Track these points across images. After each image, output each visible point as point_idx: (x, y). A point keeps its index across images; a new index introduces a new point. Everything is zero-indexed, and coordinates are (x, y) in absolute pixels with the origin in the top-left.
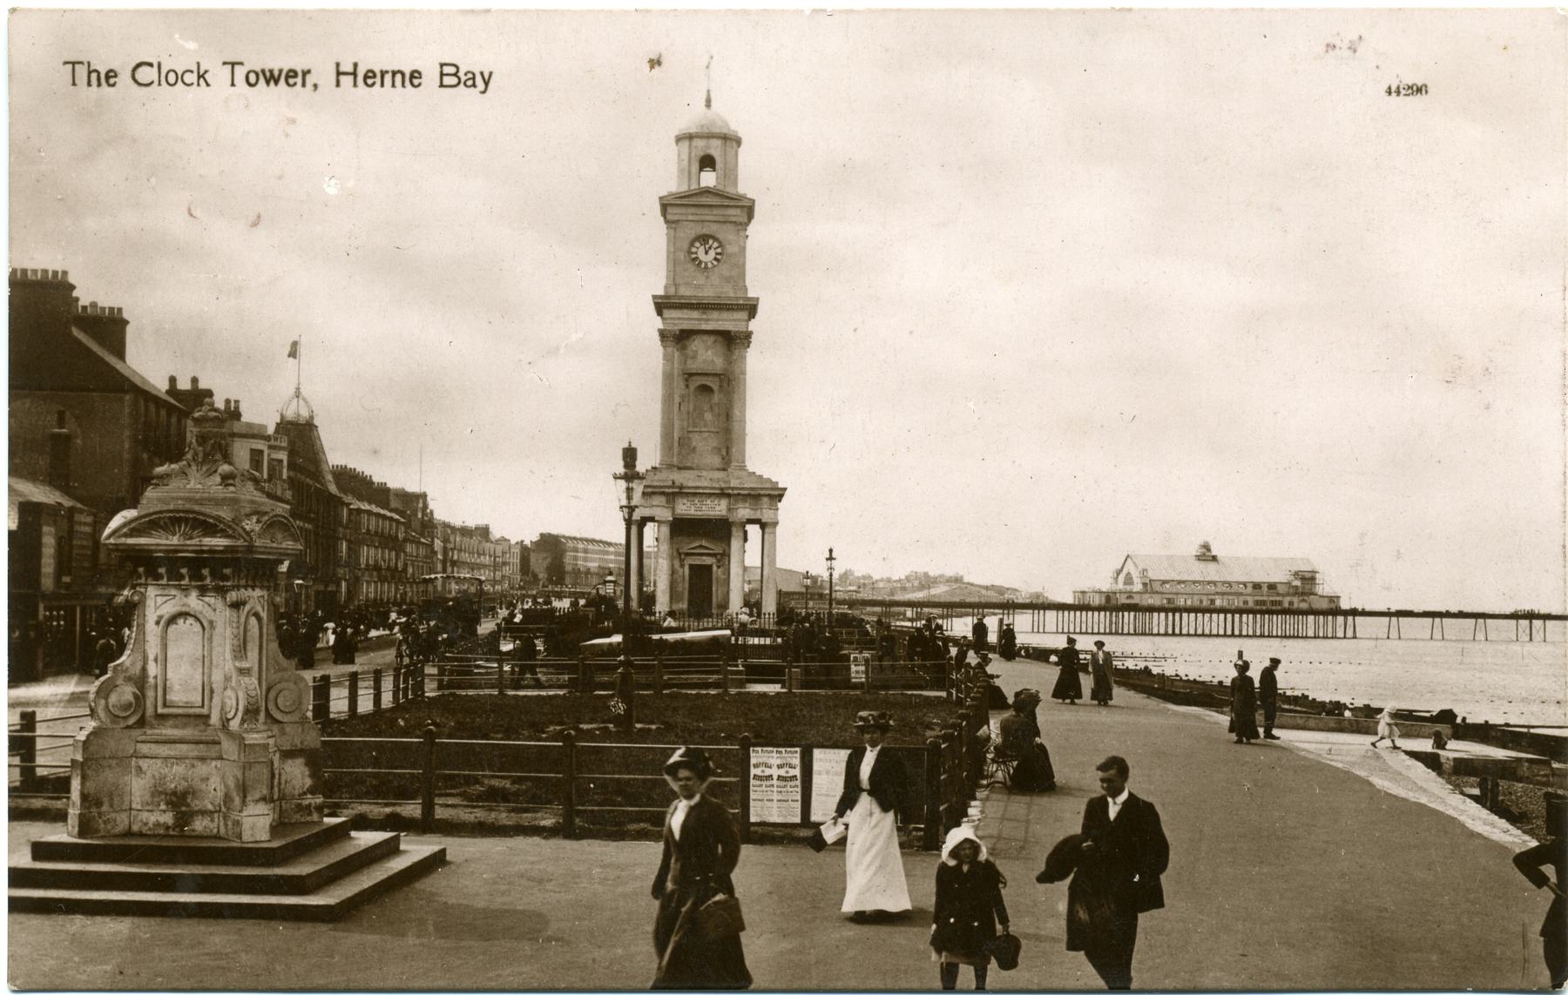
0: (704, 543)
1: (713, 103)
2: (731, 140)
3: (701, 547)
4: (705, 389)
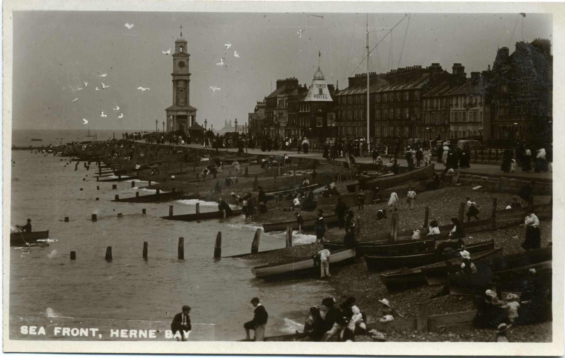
2: (185, 43)
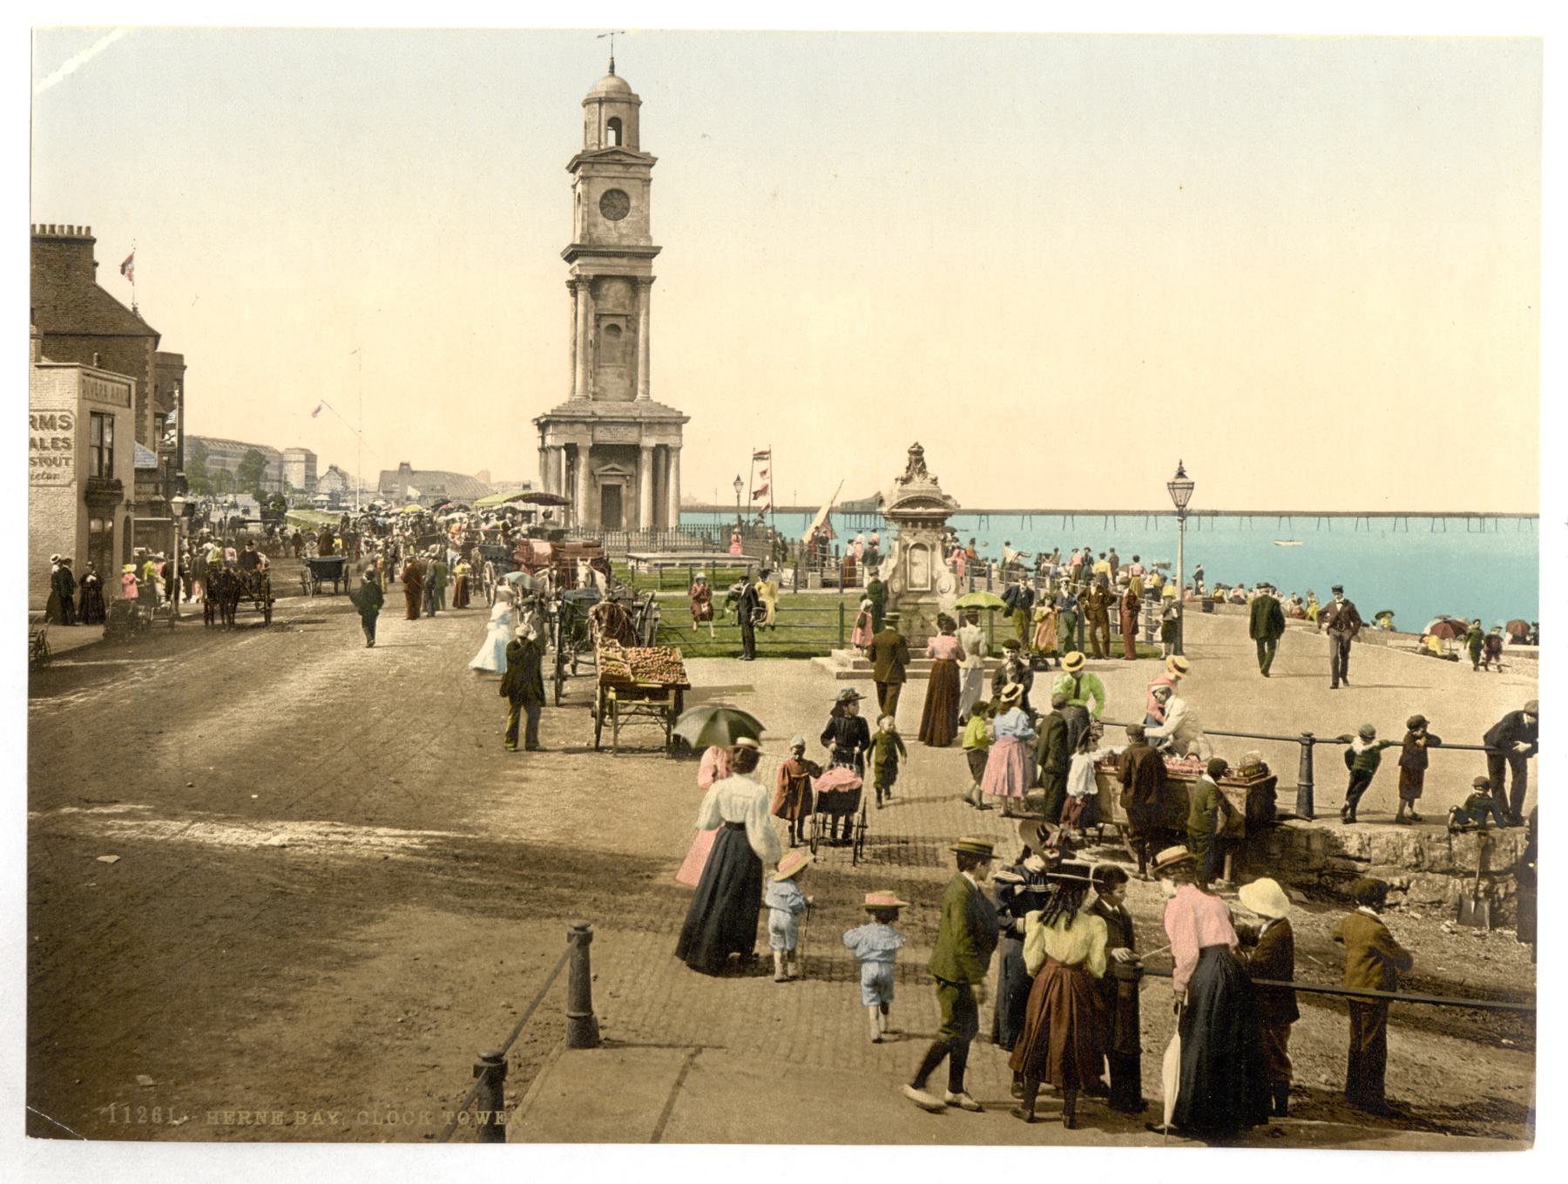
0: (617, 467)
1: (616, 70)
3: (613, 469)
4: (615, 328)
